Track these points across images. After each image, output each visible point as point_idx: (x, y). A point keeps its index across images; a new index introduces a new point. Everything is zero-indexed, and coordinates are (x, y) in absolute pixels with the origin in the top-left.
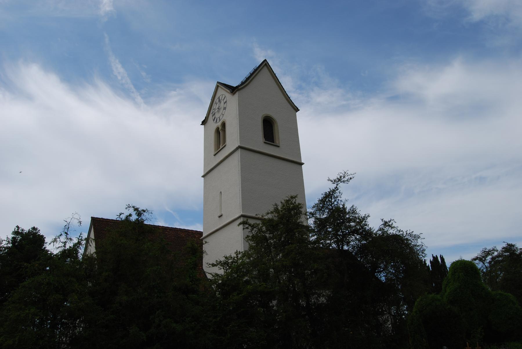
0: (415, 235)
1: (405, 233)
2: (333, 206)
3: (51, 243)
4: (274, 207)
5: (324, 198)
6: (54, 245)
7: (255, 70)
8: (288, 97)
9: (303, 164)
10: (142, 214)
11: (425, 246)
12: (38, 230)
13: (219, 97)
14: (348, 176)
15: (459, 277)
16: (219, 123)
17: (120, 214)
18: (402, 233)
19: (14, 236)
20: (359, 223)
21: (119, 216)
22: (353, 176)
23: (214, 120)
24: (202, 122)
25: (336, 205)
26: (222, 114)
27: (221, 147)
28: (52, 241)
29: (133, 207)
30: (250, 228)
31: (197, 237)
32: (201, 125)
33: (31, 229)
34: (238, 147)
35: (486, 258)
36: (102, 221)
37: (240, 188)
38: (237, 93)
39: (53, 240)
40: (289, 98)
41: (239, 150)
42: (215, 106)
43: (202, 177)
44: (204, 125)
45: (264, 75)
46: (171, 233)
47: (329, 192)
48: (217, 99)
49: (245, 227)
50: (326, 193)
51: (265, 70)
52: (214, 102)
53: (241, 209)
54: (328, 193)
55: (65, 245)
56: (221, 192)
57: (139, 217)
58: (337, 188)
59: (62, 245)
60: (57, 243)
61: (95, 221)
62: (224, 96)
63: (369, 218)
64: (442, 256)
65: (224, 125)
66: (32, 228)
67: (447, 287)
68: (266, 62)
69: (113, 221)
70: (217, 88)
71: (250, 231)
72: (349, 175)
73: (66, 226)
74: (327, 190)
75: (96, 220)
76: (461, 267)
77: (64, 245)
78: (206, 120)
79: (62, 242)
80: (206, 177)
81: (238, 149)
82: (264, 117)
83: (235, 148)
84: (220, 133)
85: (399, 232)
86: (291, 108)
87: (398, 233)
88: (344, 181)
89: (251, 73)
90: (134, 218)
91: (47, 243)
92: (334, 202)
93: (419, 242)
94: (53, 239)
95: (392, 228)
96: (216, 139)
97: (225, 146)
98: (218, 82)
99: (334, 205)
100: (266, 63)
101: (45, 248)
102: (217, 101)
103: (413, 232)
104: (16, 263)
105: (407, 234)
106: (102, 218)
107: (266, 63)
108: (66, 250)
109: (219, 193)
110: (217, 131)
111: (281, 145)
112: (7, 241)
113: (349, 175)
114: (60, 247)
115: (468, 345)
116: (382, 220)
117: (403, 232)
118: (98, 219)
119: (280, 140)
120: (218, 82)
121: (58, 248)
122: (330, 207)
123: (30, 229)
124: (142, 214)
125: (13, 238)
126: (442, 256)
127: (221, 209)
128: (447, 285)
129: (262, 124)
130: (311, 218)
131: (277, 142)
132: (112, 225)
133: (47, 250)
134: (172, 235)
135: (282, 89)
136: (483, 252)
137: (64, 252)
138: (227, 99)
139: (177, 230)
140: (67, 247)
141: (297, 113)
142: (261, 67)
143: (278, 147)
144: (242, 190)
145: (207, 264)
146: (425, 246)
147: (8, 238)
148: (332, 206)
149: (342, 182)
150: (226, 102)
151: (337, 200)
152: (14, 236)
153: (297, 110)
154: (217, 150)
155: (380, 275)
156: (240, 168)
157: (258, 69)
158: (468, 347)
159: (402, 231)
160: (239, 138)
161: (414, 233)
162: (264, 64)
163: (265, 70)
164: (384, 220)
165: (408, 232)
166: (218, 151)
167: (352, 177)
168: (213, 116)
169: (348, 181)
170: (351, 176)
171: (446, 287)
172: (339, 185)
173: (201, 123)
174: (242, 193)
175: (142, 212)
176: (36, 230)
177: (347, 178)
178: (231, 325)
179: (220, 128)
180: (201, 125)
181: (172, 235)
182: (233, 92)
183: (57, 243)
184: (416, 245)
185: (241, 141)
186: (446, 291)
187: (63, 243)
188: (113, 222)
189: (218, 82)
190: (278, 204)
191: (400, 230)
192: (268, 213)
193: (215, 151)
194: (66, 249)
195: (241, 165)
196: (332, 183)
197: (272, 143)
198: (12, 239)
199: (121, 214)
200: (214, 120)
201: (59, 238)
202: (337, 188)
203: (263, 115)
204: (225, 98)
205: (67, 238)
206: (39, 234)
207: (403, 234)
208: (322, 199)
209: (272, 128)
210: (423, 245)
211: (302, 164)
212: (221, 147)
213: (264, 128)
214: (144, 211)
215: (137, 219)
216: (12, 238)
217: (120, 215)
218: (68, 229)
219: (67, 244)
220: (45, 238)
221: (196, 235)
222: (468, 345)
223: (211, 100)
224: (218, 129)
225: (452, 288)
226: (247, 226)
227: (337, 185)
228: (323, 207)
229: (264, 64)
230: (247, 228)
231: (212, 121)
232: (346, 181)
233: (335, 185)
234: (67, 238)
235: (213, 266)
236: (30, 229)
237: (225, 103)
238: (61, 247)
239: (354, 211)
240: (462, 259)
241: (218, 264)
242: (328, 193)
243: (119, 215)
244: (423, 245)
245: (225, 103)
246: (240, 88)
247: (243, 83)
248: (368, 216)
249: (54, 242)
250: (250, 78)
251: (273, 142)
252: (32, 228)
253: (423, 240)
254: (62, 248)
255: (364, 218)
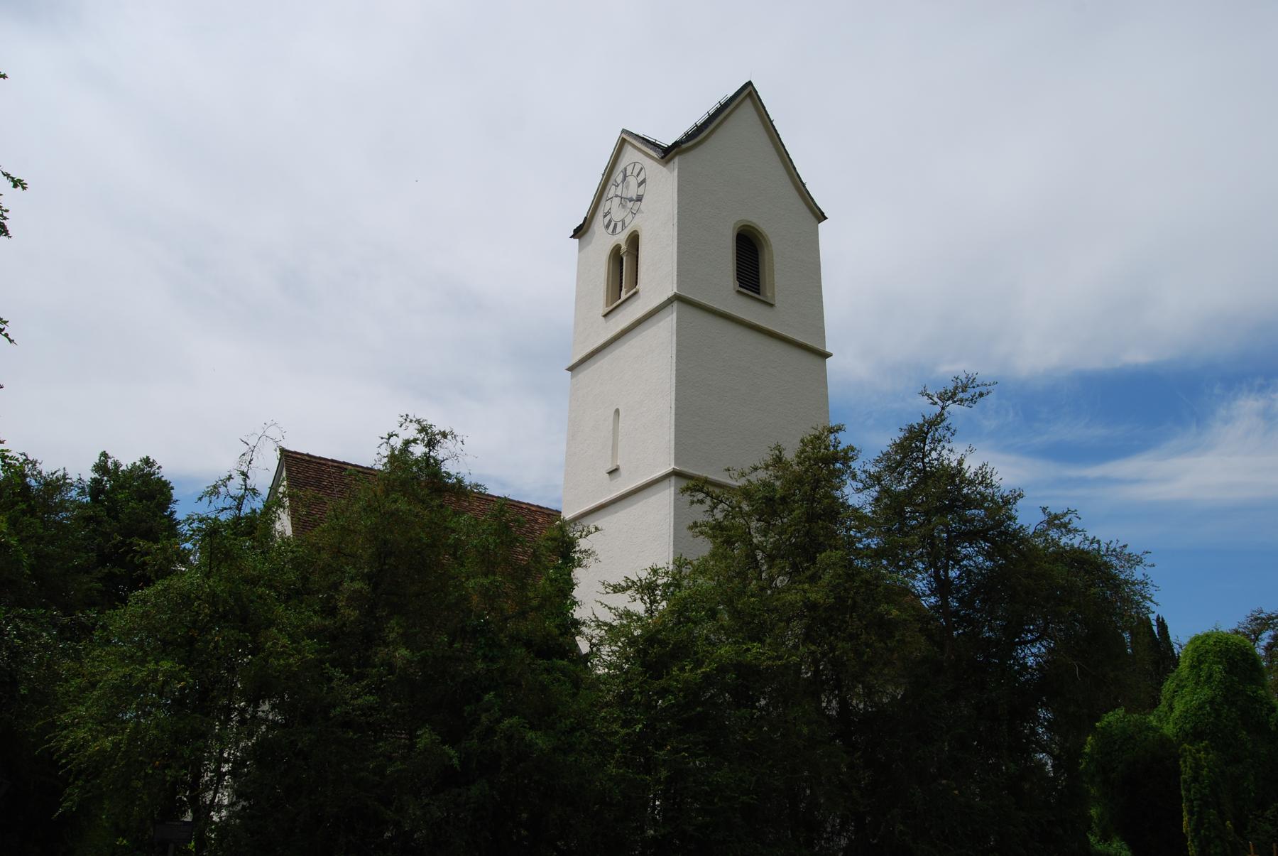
0: (1130, 554)
1: (1103, 548)
2: (927, 463)
3: (202, 497)
4: (772, 453)
5: (906, 439)
6: (210, 502)
7: (723, 107)
8: (802, 182)
9: (828, 355)
10: (439, 442)
11: (1153, 586)
12: (157, 466)
13: (625, 169)
14: (974, 387)
15: (1211, 675)
16: (621, 234)
17: (390, 436)
18: (1096, 546)
19: (97, 475)
20: (991, 513)
21: (386, 440)
22: (990, 388)
23: (607, 227)
24: (575, 230)
25: (936, 459)
26: (632, 213)
27: (624, 296)
28: (207, 492)
29: (418, 422)
30: (708, 501)
31: (540, 521)
32: (571, 237)
33: (138, 463)
34: (672, 297)
35: (1259, 635)
36: (308, 461)
37: (673, 402)
38: (676, 160)
39: (209, 489)
40: (804, 185)
41: (675, 304)
42: (611, 191)
43: (567, 370)
44: (579, 238)
45: (743, 120)
46: (478, 506)
47: (921, 426)
48: (618, 172)
49: (695, 499)
50: (912, 426)
51: (747, 108)
52: (611, 181)
53: (673, 456)
54: (917, 427)
55: (239, 504)
56: (617, 411)
57: (430, 450)
58: (940, 417)
59: (230, 502)
60: (218, 497)
61: (291, 461)
62: (640, 166)
63: (1020, 502)
64: (1162, 619)
65: (634, 240)
66: (141, 461)
67: (1177, 699)
68: (751, 87)
69: (336, 464)
70: (622, 143)
71: (707, 511)
72: (978, 386)
73: (244, 455)
74: (917, 421)
75: (293, 457)
76: (1218, 649)
77: (236, 503)
78: (585, 227)
79: (231, 497)
80: (575, 372)
81: (672, 302)
82: (741, 227)
83: (664, 298)
84: (622, 259)
85: (1092, 543)
86: (805, 207)
87: (1086, 546)
88: (961, 400)
89: (711, 112)
90: (418, 450)
91: (177, 503)
92: (930, 452)
93: (1138, 573)
94: (208, 487)
95: (1069, 531)
96: (611, 279)
97: (636, 293)
98: (624, 131)
99: (930, 460)
100: (751, 91)
101: (172, 513)
102: (619, 179)
103: (1125, 546)
104: (118, 537)
105: (1107, 551)
106: (308, 455)
107: (751, 91)
108: (242, 518)
109: (614, 411)
110: (616, 256)
111: (779, 300)
112: (79, 488)
113: (978, 386)
114: (226, 509)
115: (1252, 850)
116: (1044, 509)
117: (1100, 545)
118: (299, 456)
119: (776, 290)
120: (623, 129)
121: (222, 511)
122: (918, 464)
123: (135, 463)
124: (439, 442)
125: (94, 480)
126: (1161, 620)
127: (614, 455)
128: (1177, 691)
129: (735, 244)
130: (868, 488)
131: (769, 295)
132: (333, 473)
133: (175, 519)
134: (480, 511)
135: (786, 161)
136: (1252, 618)
137: (237, 519)
138: (647, 174)
139: (493, 501)
140: (246, 510)
141: (819, 225)
142: (736, 102)
143: (772, 305)
144: (677, 408)
145: (604, 584)
146: (1153, 586)
147: (83, 481)
148: (923, 463)
149: (955, 402)
150: (643, 181)
151: (939, 449)
152: (97, 475)
153: (821, 217)
154: (611, 305)
155: (1023, 651)
156: (674, 352)
157: (729, 105)
158: (1253, 854)
159: (1098, 542)
160: (676, 273)
161: (1127, 551)
162: (746, 92)
163: (747, 108)
164: (1048, 510)
165: (1112, 546)
166: (615, 305)
167: (985, 392)
168: (605, 216)
169: (972, 400)
170: (983, 389)
171: (1173, 697)
172: (947, 409)
173: (572, 233)
174: (676, 414)
175: (438, 437)
176: (150, 467)
177: (971, 391)
178: (669, 747)
179: (624, 247)
180: (571, 237)
181: (480, 511)
182: (667, 157)
183: (218, 497)
184: (1126, 582)
185: (678, 287)
186: (1171, 708)
187: (235, 500)
188: (335, 467)
189: (623, 129)
190: (783, 446)
191: (1095, 537)
192: (756, 469)
193: (607, 307)
194: (242, 514)
195: (678, 345)
196: (931, 401)
197: (756, 296)
198: (91, 483)
199: (392, 436)
200: (607, 227)
201: (226, 487)
202: (940, 417)
203: (739, 221)
204: (643, 170)
205: (246, 487)
206: (160, 476)
207: (1098, 550)
208: (901, 443)
209: (758, 258)
210: (1149, 581)
211: (826, 355)
212: (624, 296)
213: (737, 256)
214: (444, 435)
215: (425, 454)
216: (90, 480)
217: (389, 439)
218: (250, 463)
219: (245, 501)
220: (172, 488)
221: (539, 516)
222: (1252, 850)
223: (603, 175)
224: (616, 252)
225: (1191, 701)
226: (701, 496)
227: (943, 408)
228: (899, 464)
229: (746, 92)
230: (701, 502)
231: (603, 229)
232: (967, 400)
233: (937, 409)
234: (246, 487)
235: (615, 592)
236: (135, 463)
237: (640, 185)
238: (231, 508)
239: (984, 480)
240: (1220, 630)
241: (629, 588)
242: (916, 426)
243: (387, 437)
244: (1146, 583)
245: (640, 185)
246: (684, 146)
247: (690, 136)
248: (1019, 495)
249: (211, 494)
250: (710, 123)
251: (759, 293)
252: (141, 461)
253: (1148, 571)
254: (232, 512)
255: (575, 603)
